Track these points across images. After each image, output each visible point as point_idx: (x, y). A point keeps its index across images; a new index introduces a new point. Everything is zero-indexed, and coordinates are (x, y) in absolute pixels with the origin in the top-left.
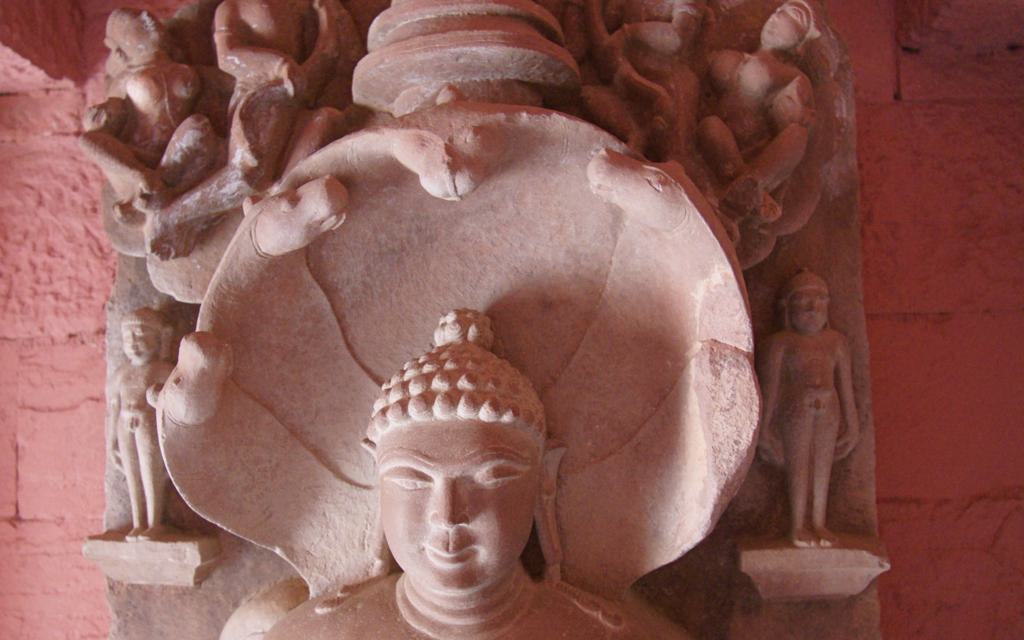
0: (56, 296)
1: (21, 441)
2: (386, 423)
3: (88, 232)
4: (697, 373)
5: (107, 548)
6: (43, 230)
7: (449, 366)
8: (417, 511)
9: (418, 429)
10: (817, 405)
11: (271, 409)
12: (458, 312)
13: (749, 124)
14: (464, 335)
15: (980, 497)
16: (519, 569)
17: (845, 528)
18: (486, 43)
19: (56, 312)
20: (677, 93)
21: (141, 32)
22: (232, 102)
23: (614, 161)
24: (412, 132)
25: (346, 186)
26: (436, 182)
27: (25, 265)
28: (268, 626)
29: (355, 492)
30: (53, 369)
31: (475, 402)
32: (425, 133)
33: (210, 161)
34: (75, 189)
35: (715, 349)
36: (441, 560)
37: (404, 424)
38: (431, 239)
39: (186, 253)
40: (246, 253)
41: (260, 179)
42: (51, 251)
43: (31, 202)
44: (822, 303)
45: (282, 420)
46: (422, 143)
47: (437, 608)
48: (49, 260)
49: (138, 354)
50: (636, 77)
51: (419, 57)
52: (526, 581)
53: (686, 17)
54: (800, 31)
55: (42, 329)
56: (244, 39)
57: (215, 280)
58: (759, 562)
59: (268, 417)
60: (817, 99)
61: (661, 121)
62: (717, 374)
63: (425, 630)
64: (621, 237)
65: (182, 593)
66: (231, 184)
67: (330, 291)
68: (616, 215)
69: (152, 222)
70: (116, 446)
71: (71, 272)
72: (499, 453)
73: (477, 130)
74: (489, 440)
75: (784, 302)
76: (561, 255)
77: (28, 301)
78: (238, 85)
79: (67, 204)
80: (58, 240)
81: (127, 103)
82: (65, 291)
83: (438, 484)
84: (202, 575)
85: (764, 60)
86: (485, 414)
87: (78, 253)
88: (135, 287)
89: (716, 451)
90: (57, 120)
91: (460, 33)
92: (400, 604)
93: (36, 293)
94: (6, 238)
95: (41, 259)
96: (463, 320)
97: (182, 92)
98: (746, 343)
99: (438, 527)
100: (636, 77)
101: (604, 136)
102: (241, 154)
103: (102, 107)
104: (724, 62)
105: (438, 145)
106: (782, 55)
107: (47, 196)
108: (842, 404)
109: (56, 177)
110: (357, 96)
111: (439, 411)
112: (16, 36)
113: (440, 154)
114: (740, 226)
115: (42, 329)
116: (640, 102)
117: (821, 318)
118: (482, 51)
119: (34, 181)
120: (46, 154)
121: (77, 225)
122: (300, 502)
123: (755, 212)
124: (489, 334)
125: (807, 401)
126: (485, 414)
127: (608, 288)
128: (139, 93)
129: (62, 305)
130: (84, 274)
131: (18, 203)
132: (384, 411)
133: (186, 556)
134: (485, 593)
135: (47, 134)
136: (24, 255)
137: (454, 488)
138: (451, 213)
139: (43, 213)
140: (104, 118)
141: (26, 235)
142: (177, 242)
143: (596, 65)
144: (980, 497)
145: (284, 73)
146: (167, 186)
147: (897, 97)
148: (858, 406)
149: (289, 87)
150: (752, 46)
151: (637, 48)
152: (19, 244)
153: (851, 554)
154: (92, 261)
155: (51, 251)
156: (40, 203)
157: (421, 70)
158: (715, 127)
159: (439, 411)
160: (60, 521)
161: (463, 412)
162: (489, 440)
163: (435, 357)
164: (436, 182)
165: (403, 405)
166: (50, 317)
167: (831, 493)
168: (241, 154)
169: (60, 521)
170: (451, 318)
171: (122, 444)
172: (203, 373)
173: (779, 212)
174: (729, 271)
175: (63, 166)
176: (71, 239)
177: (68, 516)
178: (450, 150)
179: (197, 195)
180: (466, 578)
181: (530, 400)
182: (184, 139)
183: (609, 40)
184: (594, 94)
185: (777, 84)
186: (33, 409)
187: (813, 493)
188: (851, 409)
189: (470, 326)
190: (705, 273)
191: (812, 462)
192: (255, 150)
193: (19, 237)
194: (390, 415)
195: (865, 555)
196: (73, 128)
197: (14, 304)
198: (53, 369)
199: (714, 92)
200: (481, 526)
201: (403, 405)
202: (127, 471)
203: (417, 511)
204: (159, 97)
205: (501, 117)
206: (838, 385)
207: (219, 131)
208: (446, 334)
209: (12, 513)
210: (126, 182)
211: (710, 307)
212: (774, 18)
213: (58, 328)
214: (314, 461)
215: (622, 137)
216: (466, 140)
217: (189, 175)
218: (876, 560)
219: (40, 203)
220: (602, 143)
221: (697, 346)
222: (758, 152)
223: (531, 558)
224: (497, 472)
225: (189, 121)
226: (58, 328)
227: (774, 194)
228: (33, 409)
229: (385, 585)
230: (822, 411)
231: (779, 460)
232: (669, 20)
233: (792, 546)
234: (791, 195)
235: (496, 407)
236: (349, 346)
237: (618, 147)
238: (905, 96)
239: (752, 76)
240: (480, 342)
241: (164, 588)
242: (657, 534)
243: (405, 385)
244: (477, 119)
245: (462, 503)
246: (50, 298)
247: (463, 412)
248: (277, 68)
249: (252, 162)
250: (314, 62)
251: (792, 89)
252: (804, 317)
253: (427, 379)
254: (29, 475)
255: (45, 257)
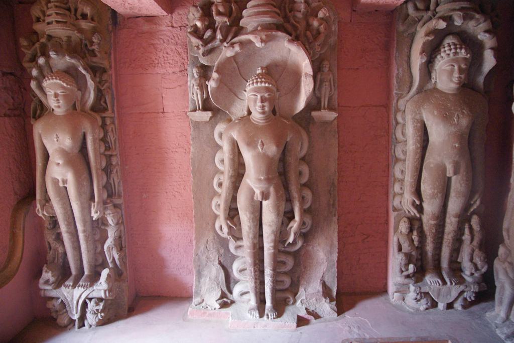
0: (169, 63)
1: (163, 95)
2: (249, 87)
3: (176, 49)
4: (303, 78)
5: (193, 113)
6: (165, 49)
7: (261, 77)
8: (255, 101)
9: (255, 88)
10: (326, 85)
11: (226, 85)
12: (262, 67)
13: (314, 32)
14: (262, 71)
15: (363, 106)
16: (272, 114)
17: (331, 108)
18: (267, 18)
19: (170, 67)
20: (301, 27)
21: (198, 11)
22: (216, 26)
23: (290, 41)
24: (254, 35)
25: (241, 44)
26: (258, 44)
27: (161, 56)
28: (225, 127)
29: (241, 101)
30: (170, 80)
31: (265, 83)
32: (257, 36)
33: (213, 38)
34: (172, 39)
35: (306, 74)
36: (259, 110)
37: (253, 87)
38: (255, 53)
39: (207, 55)
40: (224, 57)
41: (222, 41)
42: (167, 53)
43: (162, 42)
44: (328, 66)
45: (228, 87)
46: (256, 37)
47: (259, 119)
48: (167, 55)
49: (197, 75)
50: (294, 22)
51: (255, 20)
52: (273, 116)
53: (303, 12)
54: (325, 15)
55: (167, 71)
56: (219, 13)
57: (218, 60)
58: (315, 114)
59: (225, 87)
60: (328, 27)
61: (298, 32)
62: (306, 79)
63: (256, 123)
64: (290, 55)
65: (206, 122)
66: (217, 42)
67: (237, 63)
68: (290, 50)
69: (201, 51)
70: (193, 94)
71: (172, 58)
72: (269, 91)
73: (265, 35)
74: (267, 90)
75: (321, 66)
76: (279, 57)
77: (163, 64)
78: (217, 22)
79: (170, 43)
80: (169, 51)
81: (196, 25)
82: (171, 62)
83: (259, 97)
84: (211, 118)
85: (318, 20)
86: (267, 85)
87: (174, 54)
88: (194, 62)
89: (306, 92)
90: (166, 23)
91: (262, 15)
92: (252, 120)
93: (164, 63)
94: (157, 50)
95: (165, 55)
96: (262, 69)
97: (206, 23)
98: (311, 73)
99: (259, 104)
100: (294, 22)
101: (288, 36)
102: (219, 36)
103: (192, 27)
104: (311, 20)
105: (259, 38)
106: (322, 19)
107: (165, 41)
108: (331, 85)
109: (167, 36)
110: (240, 25)
111: (259, 84)
112: (164, 7)
113: (259, 40)
114: (313, 52)
115: (167, 71)
116: (295, 28)
117: (327, 69)
118: (266, 19)
119: (162, 37)
120: (164, 31)
121: (173, 47)
122: (231, 103)
123: (315, 49)
124: (267, 72)
125: (324, 84)
126: (267, 85)
127: (289, 59)
128: (199, 24)
129: (171, 65)
130: (175, 58)
131: (158, 42)
132: (249, 85)
133: (209, 114)
134: (266, 116)
135: (164, 26)
136: (161, 54)
137: (261, 97)
138: (260, 49)
139: (165, 45)
140: (192, 29)
141: (161, 50)
142: (207, 53)
143: (286, 18)
144: (363, 106)
145: (227, 20)
146: (206, 42)
147: (351, 21)
148: (334, 86)
149: (228, 23)
150: (316, 16)
151: (295, 17)
152: (160, 52)
153: (331, 112)
154: (177, 56)
155: (167, 53)
156: (164, 42)
157: (254, 22)
158: (308, 33)
159: (259, 84)
160: (173, 112)
161: (263, 85)
162: (267, 90)
163: (258, 75)
164: (258, 44)
165: (253, 83)
166: (168, 68)
167: (329, 102)
168: (219, 36)
169: (173, 112)
170: (260, 68)
171: (194, 94)
172: (218, 78)
173: (320, 49)
174: (308, 61)
175: (169, 34)
176: (172, 51)
177: (175, 111)
178: (261, 39)
179: (211, 44)
180: (263, 113)
181: (273, 82)
182: (208, 34)
183: (289, 14)
184: (288, 26)
185: (321, 24)
186: (166, 88)
187: (325, 102)
188: (333, 87)
189: (30, 82)
190: (305, 61)
191: (325, 96)
192: (222, 36)
193: (160, 50)
194: (251, 85)
195: (334, 113)
196: (170, 25)
197: (160, 65)
198: (170, 80)
199: (309, 26)
200: (266, 104)
201: (253, 83)
202: (196, 99)
203: (255, 101)
204: (202, 25)
205: (270, 33)
206: (330, 81)
207: (215, 31)
208: (259, 71)
209: (162, 111)
210: (195, 41)
211: (306, 66)
212: (320, 11)
213: (170, 71)
214: (233, 95)
215: (290, 35)
216: (264, 37)
217: (209, 40)
218: (335, 114)
219: (164, 42)
220: (287, 37)
221: (303, 74)
222: (316, 38)
223: (274, 112)
224: (269, 95)
225: (209, 30)
226: (170, 71)
227: (319, 45)
228: (166, 88)
229: (248, 117)
230: (327, 86)
231: (319, 95)
232: (300, 11)
233: (320, 111)
234: (322, 46)
235: (269, 84)
236: (240, 73)
237: (290, 38)
238: (352, 21)
239: (315, 23)
240: (265, 73)
241: (202, 122)
242: (296, 108)
243: (253, 80)
244: (266, 33)
245: (263, 100)
246: (168, 64)
247: (263, 85)
248: (226, 19)
249: (221, 38)
250: (232, 18)
251: (322, 26)
252: (324, 69)
253: (257, 79)
254: (166, 103)
255: (166, 55)
